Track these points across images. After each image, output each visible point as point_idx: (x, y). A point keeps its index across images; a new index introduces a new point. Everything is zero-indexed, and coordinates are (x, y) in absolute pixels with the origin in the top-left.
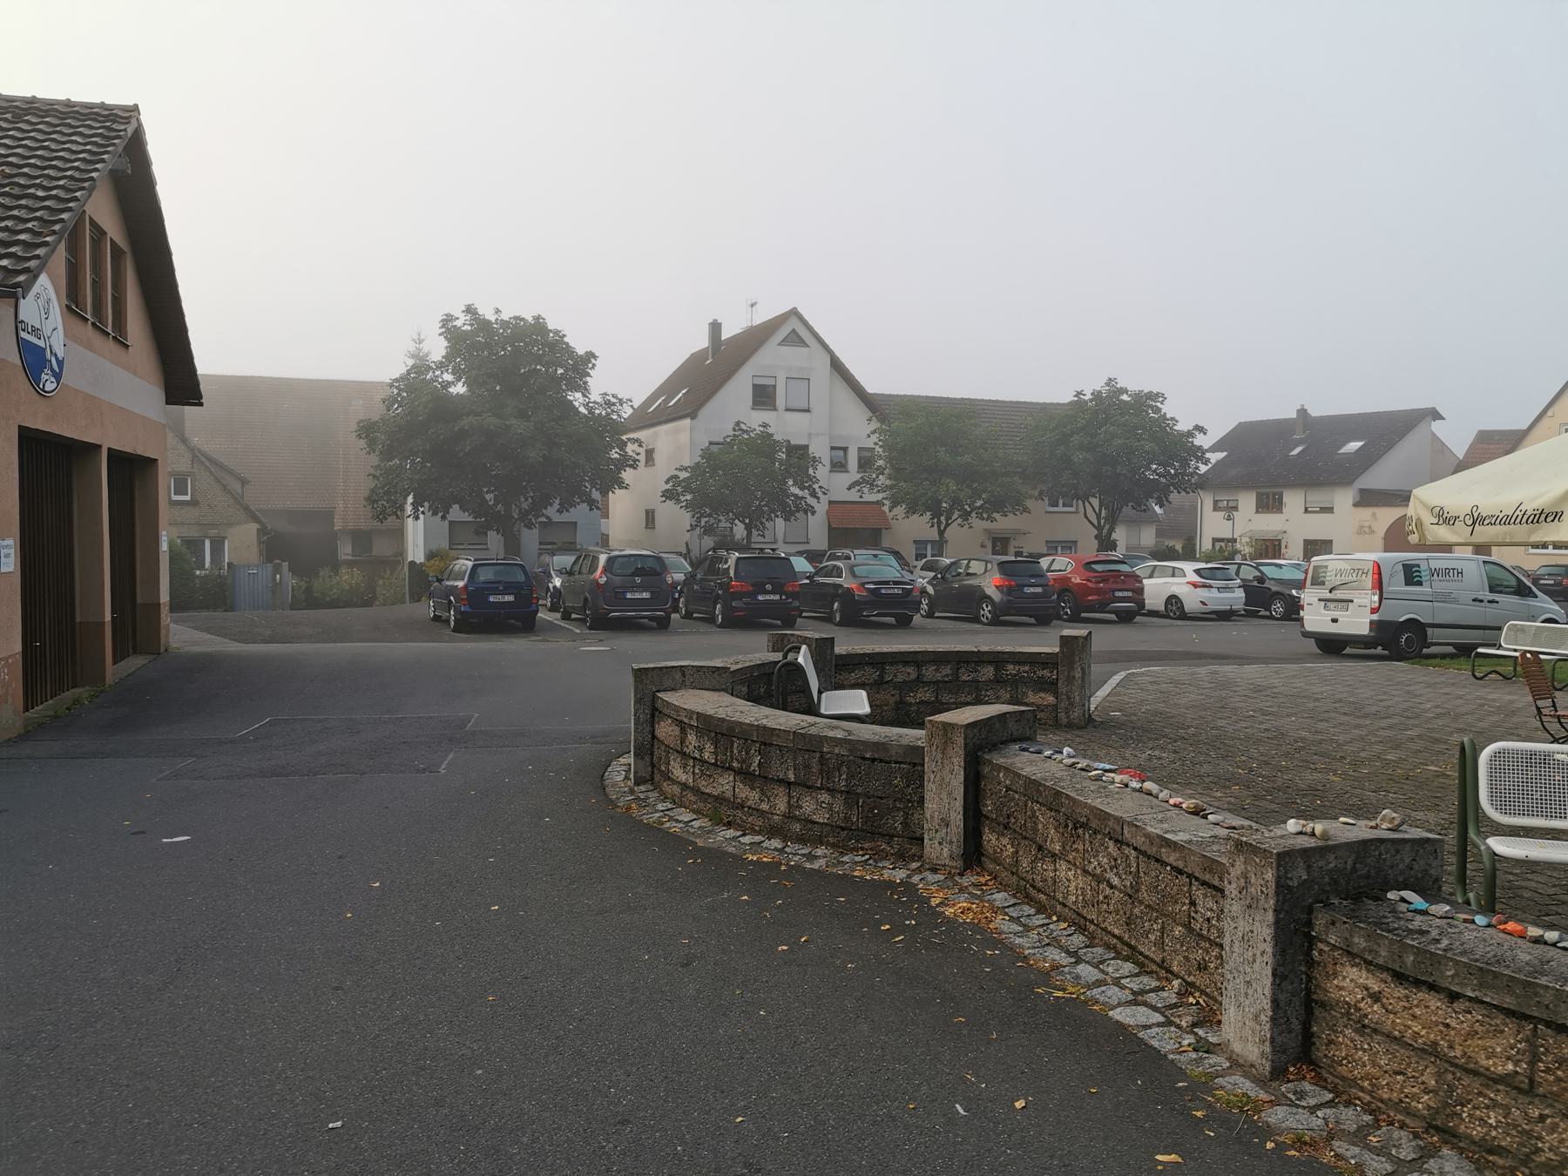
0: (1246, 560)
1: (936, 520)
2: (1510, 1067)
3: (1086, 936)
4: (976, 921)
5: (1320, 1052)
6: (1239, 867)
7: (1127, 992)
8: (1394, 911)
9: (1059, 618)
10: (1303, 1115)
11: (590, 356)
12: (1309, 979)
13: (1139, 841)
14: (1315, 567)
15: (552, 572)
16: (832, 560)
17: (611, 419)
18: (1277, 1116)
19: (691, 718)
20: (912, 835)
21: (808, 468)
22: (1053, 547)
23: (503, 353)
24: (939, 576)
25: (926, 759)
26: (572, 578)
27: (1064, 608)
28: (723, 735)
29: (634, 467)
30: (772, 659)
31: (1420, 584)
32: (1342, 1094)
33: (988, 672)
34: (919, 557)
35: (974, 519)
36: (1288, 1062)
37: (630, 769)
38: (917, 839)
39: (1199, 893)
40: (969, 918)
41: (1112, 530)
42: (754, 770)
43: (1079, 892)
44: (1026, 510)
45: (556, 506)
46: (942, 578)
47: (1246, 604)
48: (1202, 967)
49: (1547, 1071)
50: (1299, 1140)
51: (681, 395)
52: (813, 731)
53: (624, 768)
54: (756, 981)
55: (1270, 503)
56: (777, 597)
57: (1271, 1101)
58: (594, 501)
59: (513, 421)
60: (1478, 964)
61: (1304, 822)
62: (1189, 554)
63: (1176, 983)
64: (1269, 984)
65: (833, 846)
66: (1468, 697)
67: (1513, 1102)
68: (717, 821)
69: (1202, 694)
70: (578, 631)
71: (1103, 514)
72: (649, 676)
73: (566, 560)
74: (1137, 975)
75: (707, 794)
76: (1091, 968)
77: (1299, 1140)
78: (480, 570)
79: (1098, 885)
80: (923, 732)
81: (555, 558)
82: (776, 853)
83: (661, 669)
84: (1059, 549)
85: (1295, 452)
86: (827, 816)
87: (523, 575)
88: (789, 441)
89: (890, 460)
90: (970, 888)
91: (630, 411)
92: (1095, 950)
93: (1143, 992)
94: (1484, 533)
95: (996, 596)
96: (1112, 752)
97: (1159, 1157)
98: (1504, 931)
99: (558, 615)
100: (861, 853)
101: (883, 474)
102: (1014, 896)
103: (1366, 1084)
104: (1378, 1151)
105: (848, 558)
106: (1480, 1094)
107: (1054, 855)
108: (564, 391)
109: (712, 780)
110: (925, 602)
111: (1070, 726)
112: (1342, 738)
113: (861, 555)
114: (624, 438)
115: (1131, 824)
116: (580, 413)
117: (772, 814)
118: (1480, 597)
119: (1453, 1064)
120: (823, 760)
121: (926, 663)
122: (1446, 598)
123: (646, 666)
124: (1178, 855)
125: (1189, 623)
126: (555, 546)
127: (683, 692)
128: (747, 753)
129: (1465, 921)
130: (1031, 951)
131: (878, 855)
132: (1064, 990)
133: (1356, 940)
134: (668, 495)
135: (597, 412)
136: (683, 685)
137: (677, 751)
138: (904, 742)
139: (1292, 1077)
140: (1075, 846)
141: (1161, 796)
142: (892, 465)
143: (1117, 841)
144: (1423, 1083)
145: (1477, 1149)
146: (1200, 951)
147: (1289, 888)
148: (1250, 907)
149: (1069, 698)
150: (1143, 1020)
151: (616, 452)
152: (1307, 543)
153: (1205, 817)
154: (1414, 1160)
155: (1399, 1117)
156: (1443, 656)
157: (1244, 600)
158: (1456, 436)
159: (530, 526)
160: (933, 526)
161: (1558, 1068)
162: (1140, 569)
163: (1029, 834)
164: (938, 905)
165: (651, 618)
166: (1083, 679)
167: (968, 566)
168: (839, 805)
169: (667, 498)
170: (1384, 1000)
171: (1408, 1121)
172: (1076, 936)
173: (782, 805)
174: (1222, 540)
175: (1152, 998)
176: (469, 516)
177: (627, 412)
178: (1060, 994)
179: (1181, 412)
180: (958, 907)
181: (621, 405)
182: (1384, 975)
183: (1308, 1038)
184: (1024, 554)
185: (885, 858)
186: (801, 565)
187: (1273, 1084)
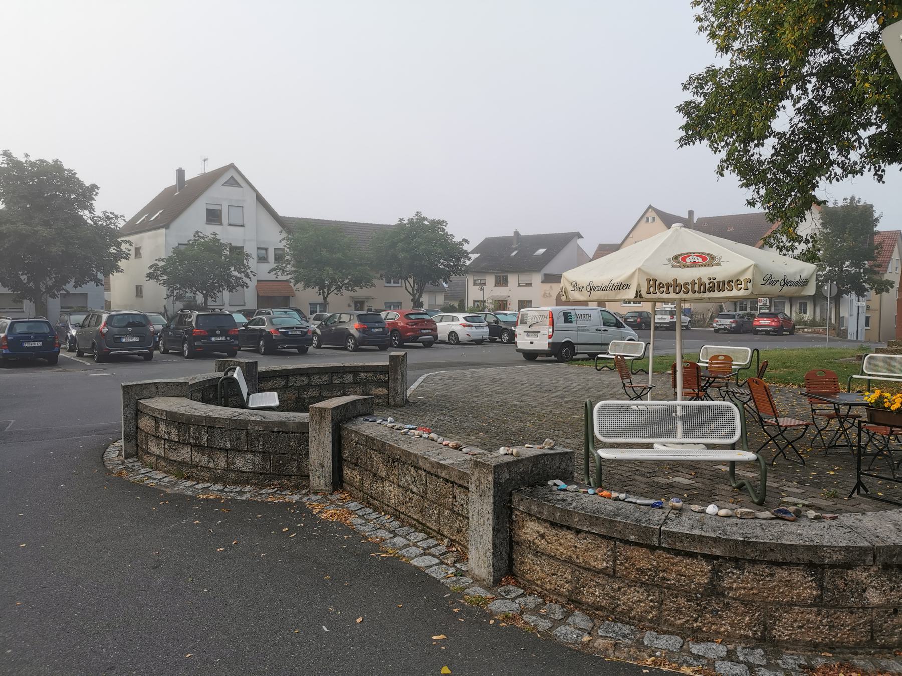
0: (490, 312)
1: (321, 291)
2: (605, 564)
3: (400, 522)
4: (339, 520)
5: (516, 569)
6: (476, 475)
7: (421, 549)
8: (551, 491)
9: (393, 346)
10: (508, 603)
11: (94, 187)
12: (511, 531)
13: (427, 466)
14: (522, 315)
15: (69, 326)
16: (259, 315)
17: (110, 228)
18: (497, 606)
19: (162, 414)
20: (303, 474)
21: (243, 260)
22: (389, 306)
23: (31, 183)
24: (323, 323)
25: (310, 429)
26: (84, 330)
27: (394, 340)
28: (183, 423)
29: (127, 258)
30: (218, 376)
31: (571, 322)
32: (528, 591)
33: (349, 378)
34: (312, 313)
35: (343, 291)
37: (122, 449)
38: (306, 476)
39: (457, 491)
40: (335, 519)
41: (420, 296)
42: (205, 444)
43: (396, 497)
44: (373, 285)
45: (72, 283)
46: (325, 324)
48: (459, 531)
49: (621, 564)
50: (506, 617)
51: (158, 214)
52: (242, 417)
53: (118, 448)
54: (202, 572)
55: (501, 282)
56: (224, 338)
57: (493, 598)
58: (99, 280)
59: (39, 228)
60: (589, 514)
61: (507, 448)
62: (461, 309)
63: (446, 541)
64: (491, 536)
65: (255, 484)
66: (593, 379)
67: (606, 582)
68: (181, 476)
69: (466, 384)
70: (88, 364)
71: (416, 288)
72: (134, 390)
73: (79, 318)
74: (426, 539)
75: (174, 460)
76: (402, 539)
77: (506, 617)
78: (15, 326)
79: (406, 493)
80: (308, 414)
81: (71, 317)
82: (219, 492)
83: (141, 385)
84: (392, 307)
85: (513, 254)
86: (251, 467)
87: (47, 327)
88: (231, 244)
89: (294, 256)
90: (336, 502)
91: (123, 223)
92: (404, 529)
93: (429, 548)
94: (597, 295)
97: (434, 638)
98: (601, 496)
99: (74, 354)
100: (272, 487)
101: (290, 264)
102: (361, 503)
103: (539, 582)
104: (544, 617)
105: (269, 314)
106: (592, 580)
107: (382, 478)
108: (76, 209)
109: (177, 451)
110: (315, 339)
111: (396, 406)
112: (534, 404)
113: (277, 312)
114: (119, 240)
115: (423, 457)
116: (87, 223)
117: (216, 469)
118: (599, 329)
120: (248, 434)
121: (313, 374)
122: (584, 329)
123: (131, 384)
124: (446, 472)
125: (461, 346)
126: (72, 310)
127: (157, 398)
128: (200, 433)
129: (584, 492)
131: (282, 488)
133: (533, 507)
134: (150, 276)
135: (100, 223)
136: (157, 394)
137: (153, 436)
138: (297, 420)
139: (503, 584)
140: (393, 472)
141: (439, 440)
142: (295, 259)
143: (415, 467)
144: (565, 578)
145: (591, 609)
146: (458, 522)
148: (481, 496)
149: (395, 390)
150: (428, 563)
151: (114, 249)
152: (520, 302)
153: (461, 450)
154: (562, 619)
155: (555, 597)
156: (583, 359)
157: (488, 333)
158: (589, 245)
159: (53, 296)
160: (320, 295)
161: (626, 562)
162: (435, 318)
163: (369, 467)
164: (317, 513)
165: (139, 354)
167: (340, 318)
168: (258, 460)
169: (150, 278)
170: (546, 537)
171: (559, 599)
172: (394, 522)
173: (222, 464)
174: (478, 301)
175: (433, 551)
176: (9, 289)
177: (121, 224)
178: (384, 555)
179: (456, 231)
180: (329, 513)
181: (117, 219)
182: (546, 524)
183: (511, 561)
184: (373, 310)
185: (287, 489)
186: (239, 319)
187: (495, 589)
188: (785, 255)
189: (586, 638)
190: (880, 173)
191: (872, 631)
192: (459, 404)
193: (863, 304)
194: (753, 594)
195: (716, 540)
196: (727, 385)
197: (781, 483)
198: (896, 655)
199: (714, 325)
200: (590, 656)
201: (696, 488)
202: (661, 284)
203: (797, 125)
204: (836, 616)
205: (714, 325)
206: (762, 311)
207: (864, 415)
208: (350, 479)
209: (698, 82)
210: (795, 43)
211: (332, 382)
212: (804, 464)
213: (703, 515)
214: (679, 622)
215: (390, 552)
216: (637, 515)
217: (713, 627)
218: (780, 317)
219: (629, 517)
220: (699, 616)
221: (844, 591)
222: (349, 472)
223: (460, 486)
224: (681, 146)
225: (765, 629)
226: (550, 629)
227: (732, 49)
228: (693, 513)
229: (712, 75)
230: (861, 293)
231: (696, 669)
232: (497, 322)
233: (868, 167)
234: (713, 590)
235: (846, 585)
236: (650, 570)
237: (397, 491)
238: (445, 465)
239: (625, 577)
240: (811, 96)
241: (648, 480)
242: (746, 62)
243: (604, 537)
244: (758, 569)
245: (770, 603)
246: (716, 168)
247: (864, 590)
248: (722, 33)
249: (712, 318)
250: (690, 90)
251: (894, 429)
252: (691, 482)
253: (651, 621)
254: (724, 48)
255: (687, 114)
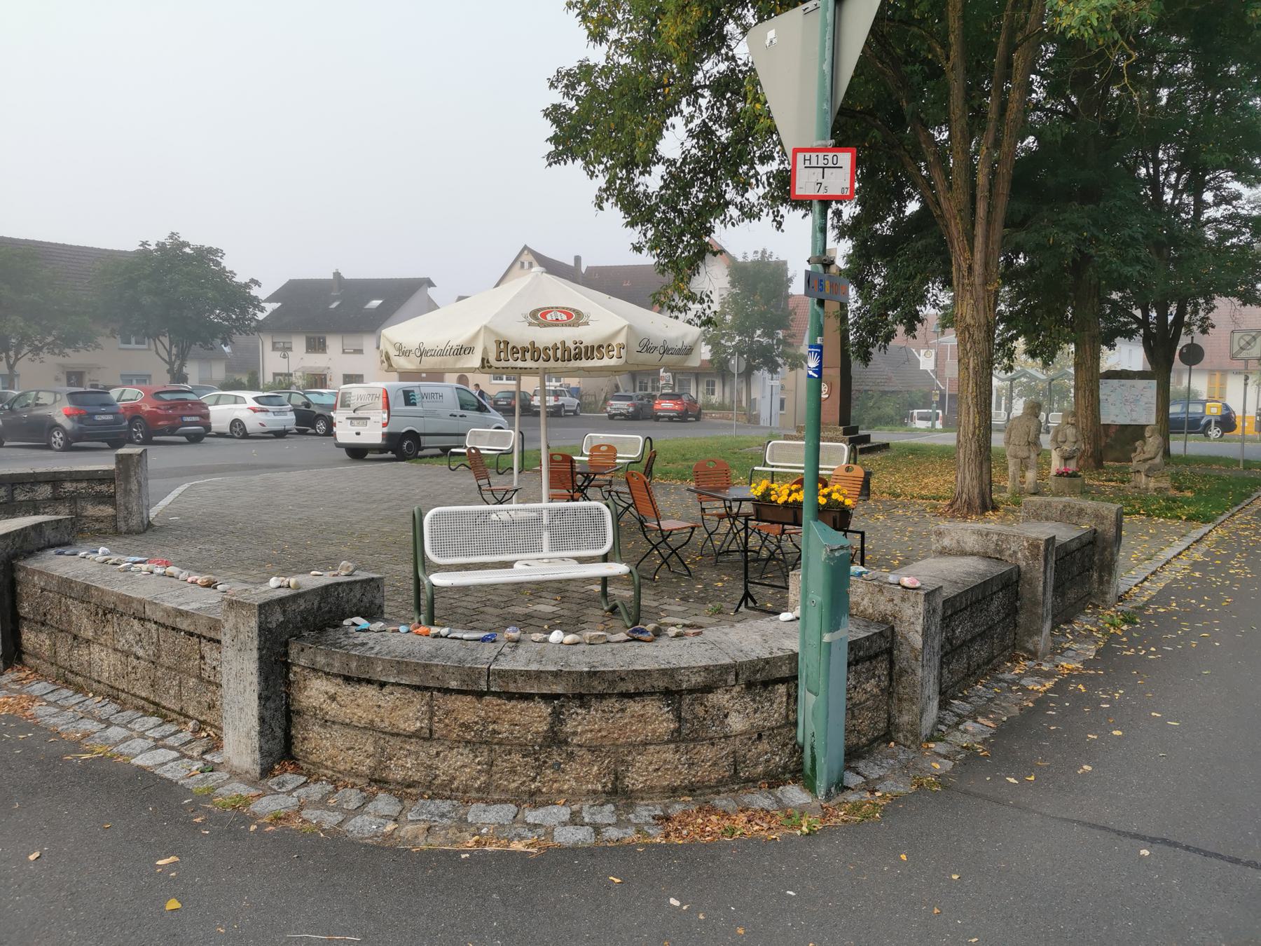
5: (298, 749)
6: (232, 620)
8: (347, 633)
12: (288, 696)
13: (158, 616)
22: (128, 380)
24: (7, 407)
27: (135, 433)
31: (414, 404)
32: (312, 777)
33: (45, 491)
36: (274, 762)
39: (206, 648)
41: (182, 365)
47: (297, 424)
48: (211, 707)
62: (253, 385)
74: (160, 725)
85: (334, 305)
90: (9, 685)
92: (124, 714)
95: (67, 424)
96: (167, 549)
97: (160, 863)
98: (417, 634)
102: (54, 683)
103: (329, 763)
107: (88, 641)
111: (129, 532)
115: (151, 603)
119: (385, 733)
122: (433, 414)
129: (393, 631)
130: (64, 727)
132: (92, 752)
133: (318, 659)
141: (181, 576)
143: (140, 619)
147: (270, 630)
148: (240, 650)
149: (127, 508)
150: (160, 759)
155: (352, 780)
156: (432, 456)
157: (294, 421)
162: (204, 398)
166: (139, 490)
174: (281, 374)
175: (171, 741)
178: (88, 756)
183: (288, 740)
187: (262, 782)
188: (677, 317)
189: (390, 826)
190: (778, 219)
191: (735, 763)
192: (238, 526)
193: (776, 383)
194: (602, 737)
195: (557, 675)
196: (610, 483)
197: (661, 601)
198: (760, 788)
199: (609, 409)
200: (395, 851)
201: (560, 617)
202: (513, 348)
203: (689, 151)
204: (696, 751)
205: (609, 409)
206: (664, 391)
207: (747, 508)
208: (35, 648)
209: (569, 79)
210: (677, 40)
211: (13, 499)
212: (690, 575)
213: (544, 645)
214: (513, 785)
215: (98, 750)
216: (461, 654)
217: (555, 785)
218: (685, 398)
219: (449, 658)
220: (538, 774)
221: (705, 719)
222: (32, 636)
223: (210, 640)
224: (550, 165)
225: (617, 778)
226: (340, 824)
227: (608, 40)
228: (533, 644)
229: (586, 72)
230: (773, 369)
231: (530, 842)
232: (308, 405)
233: (765, 210)
234: (555, 739)
235: (706, 712)
236: (477, 723)
237: (113, 658)
238: (187, 612)
239: (445, 737)
240: (705, 116)
241: (501, 612)
242: (629, 60)
243: (417, 688)
244: (607, 704)
245: (622, 745)
246: (594, 199)
247: (726, 716)
248: (595, 15)
249: (606, 400)
250: (559, 90)
251: (786, 527)
252: (555, 609)
253: (479, 790)
254: (597, 36)
255: (556, 121)
